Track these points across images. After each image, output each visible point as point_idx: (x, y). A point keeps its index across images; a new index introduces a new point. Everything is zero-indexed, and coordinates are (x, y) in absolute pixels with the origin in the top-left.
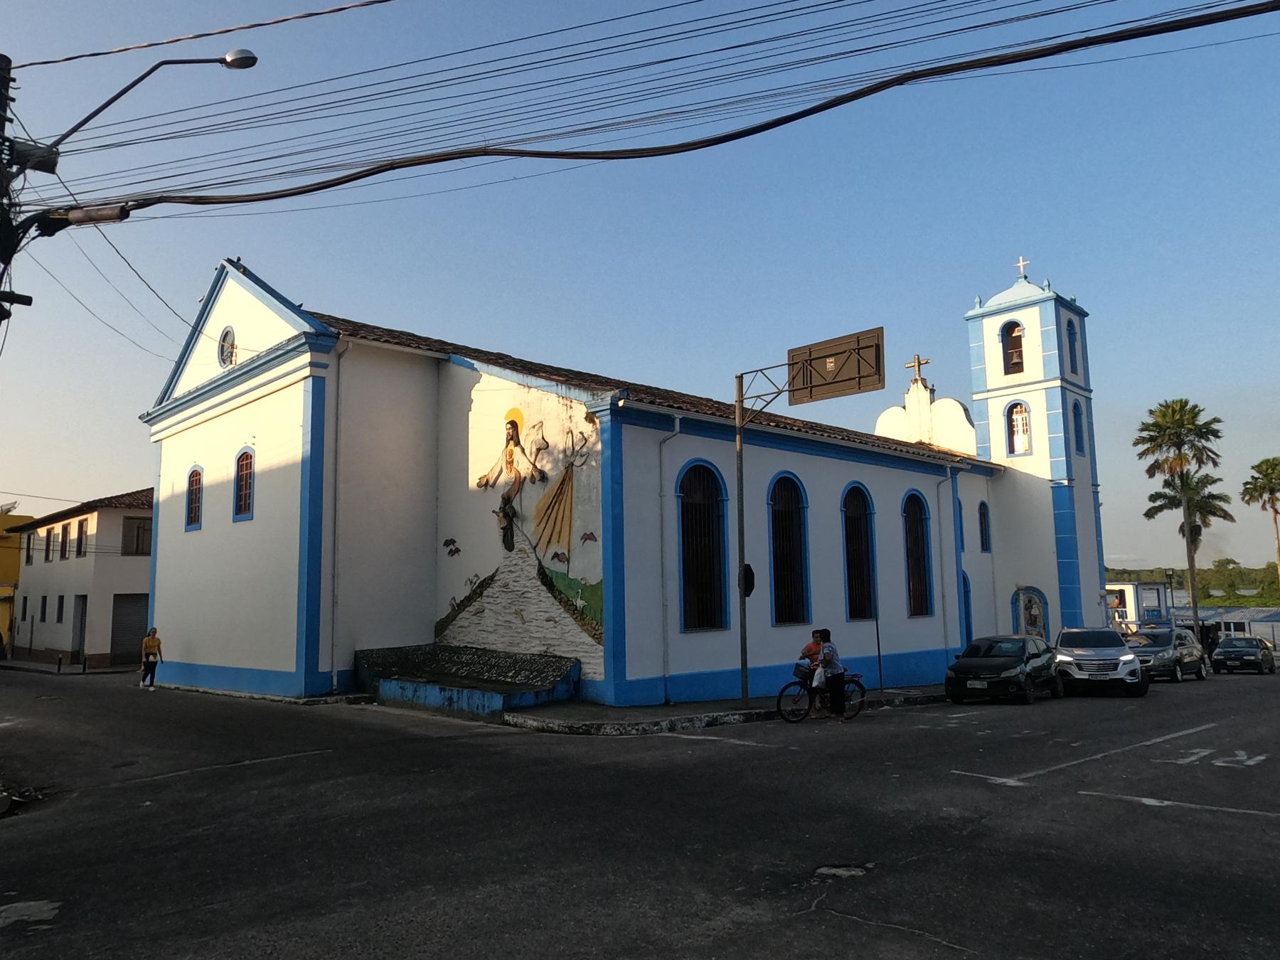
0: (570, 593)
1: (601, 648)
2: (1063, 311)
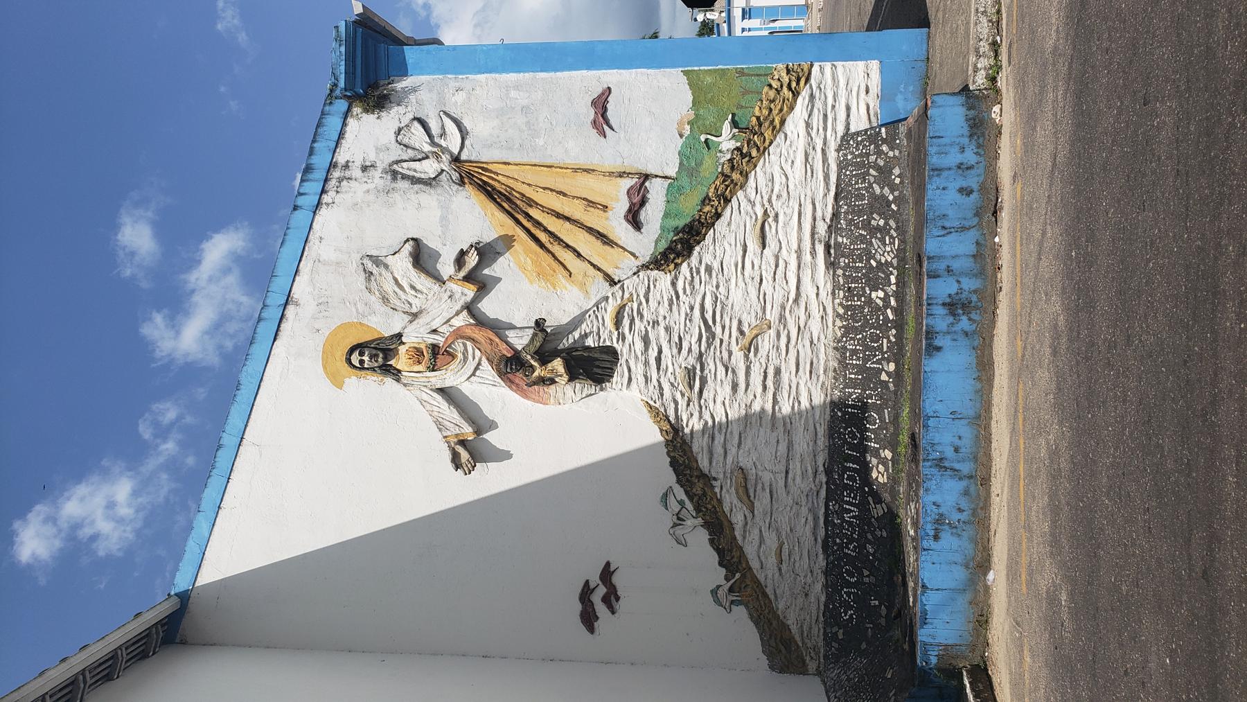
0: (711, 167)
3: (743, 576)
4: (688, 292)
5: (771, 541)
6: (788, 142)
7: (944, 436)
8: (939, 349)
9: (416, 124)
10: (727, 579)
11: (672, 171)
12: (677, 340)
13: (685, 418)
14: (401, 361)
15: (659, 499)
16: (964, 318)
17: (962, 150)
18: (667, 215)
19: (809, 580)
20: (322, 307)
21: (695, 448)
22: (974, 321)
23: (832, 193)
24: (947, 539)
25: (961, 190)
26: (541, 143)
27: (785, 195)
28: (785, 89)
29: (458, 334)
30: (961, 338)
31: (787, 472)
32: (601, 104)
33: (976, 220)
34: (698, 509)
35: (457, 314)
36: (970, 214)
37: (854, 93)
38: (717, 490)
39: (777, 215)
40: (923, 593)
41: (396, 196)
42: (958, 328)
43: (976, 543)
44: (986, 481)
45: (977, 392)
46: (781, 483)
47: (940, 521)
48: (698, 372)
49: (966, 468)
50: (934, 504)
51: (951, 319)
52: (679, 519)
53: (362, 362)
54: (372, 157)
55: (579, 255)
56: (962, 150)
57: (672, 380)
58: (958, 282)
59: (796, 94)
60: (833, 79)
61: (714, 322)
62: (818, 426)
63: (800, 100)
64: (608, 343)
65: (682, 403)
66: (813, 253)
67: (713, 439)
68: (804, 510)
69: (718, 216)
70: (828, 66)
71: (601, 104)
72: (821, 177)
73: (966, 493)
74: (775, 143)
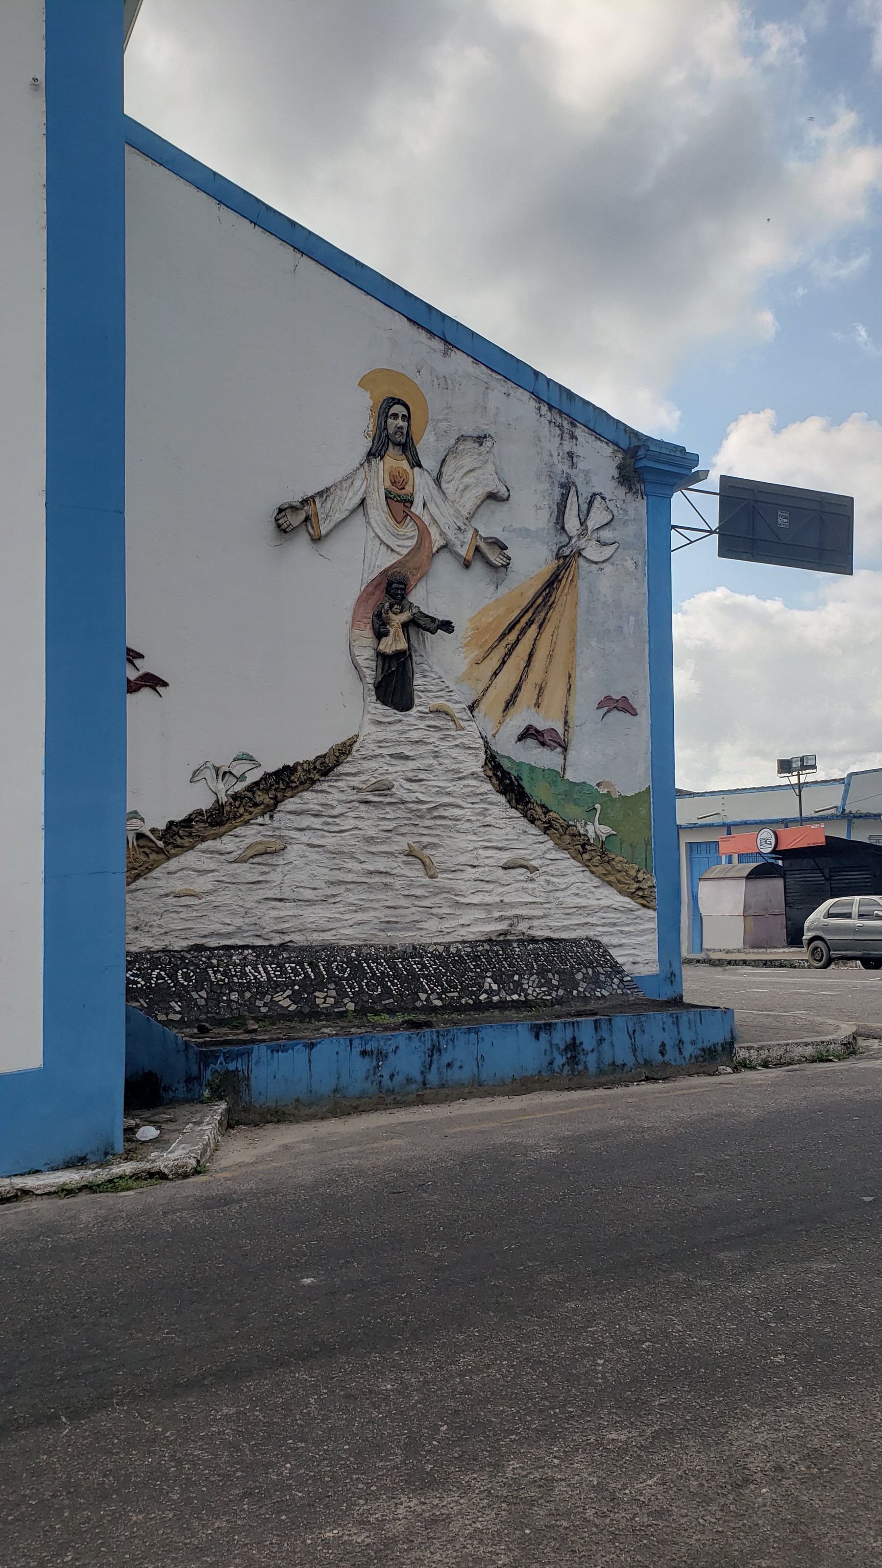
0: (570, 812)
1: (653, 914)
2: (394, 505)
3: (160, 851)
4: (465, 790)
5: (202, 884)
6: (593, 890)
7: (461, 1051)
8: (537, 1037)
9: (610, 517)
10: (153, 831)
11: (570, 776)
12: (421, 777)
13: (339, 784)
14: (394, 461)
15: (245, 751)
16: (564, 1060)
17: (693, 1043)
18: (532, 769)
19: (155, 931)
20: (442, 381)
21: (307, 795)
22: (562, 1070)
23: (555, 936)
24: (364, 1065)
25: (663, 1045)
26: (592, 643)
27: (550, 888)
28: (636, 885)
29: (423, 533)
30: (548, 1059)
31: (281, 900)
32: (624, 706)
33: (642, 1062)
34: (236, 797)
35: (442, 534)
36: (646, 1056)
37: (632, 951)
38: (260, 820)
39: (532, 880)
40: (305, 1045)
41: (547, 486)
42: (556, 1054)
43: (359, 1098)
44: (422, 1101)
45: (502, 1080)
46: (270, 894)
47: (381, 1055)
48: (389, 800)
49: (433, 1077)
50: (397, 1047)
51: (562, 1047)
52: (225, 773)
53: (395, 416)
54: (581, 465)
55: (496, 674)
56: (693, 1043)
57: (381, 771)
58: (593, 1051)
59: (632, 895)
60: (644, 931)
61: (435, 818)
62: (334, 932)
63: (628, 900)
64: (417, 701)
65: (356, 781)
66: (501, 919)
67: (316, 816)
68: (238, 922)
69: (532, 821)
70: (654, 925)
71: (624, 706)
72: (566, 923)
73: (409, 1080)
74: (592, 876)
